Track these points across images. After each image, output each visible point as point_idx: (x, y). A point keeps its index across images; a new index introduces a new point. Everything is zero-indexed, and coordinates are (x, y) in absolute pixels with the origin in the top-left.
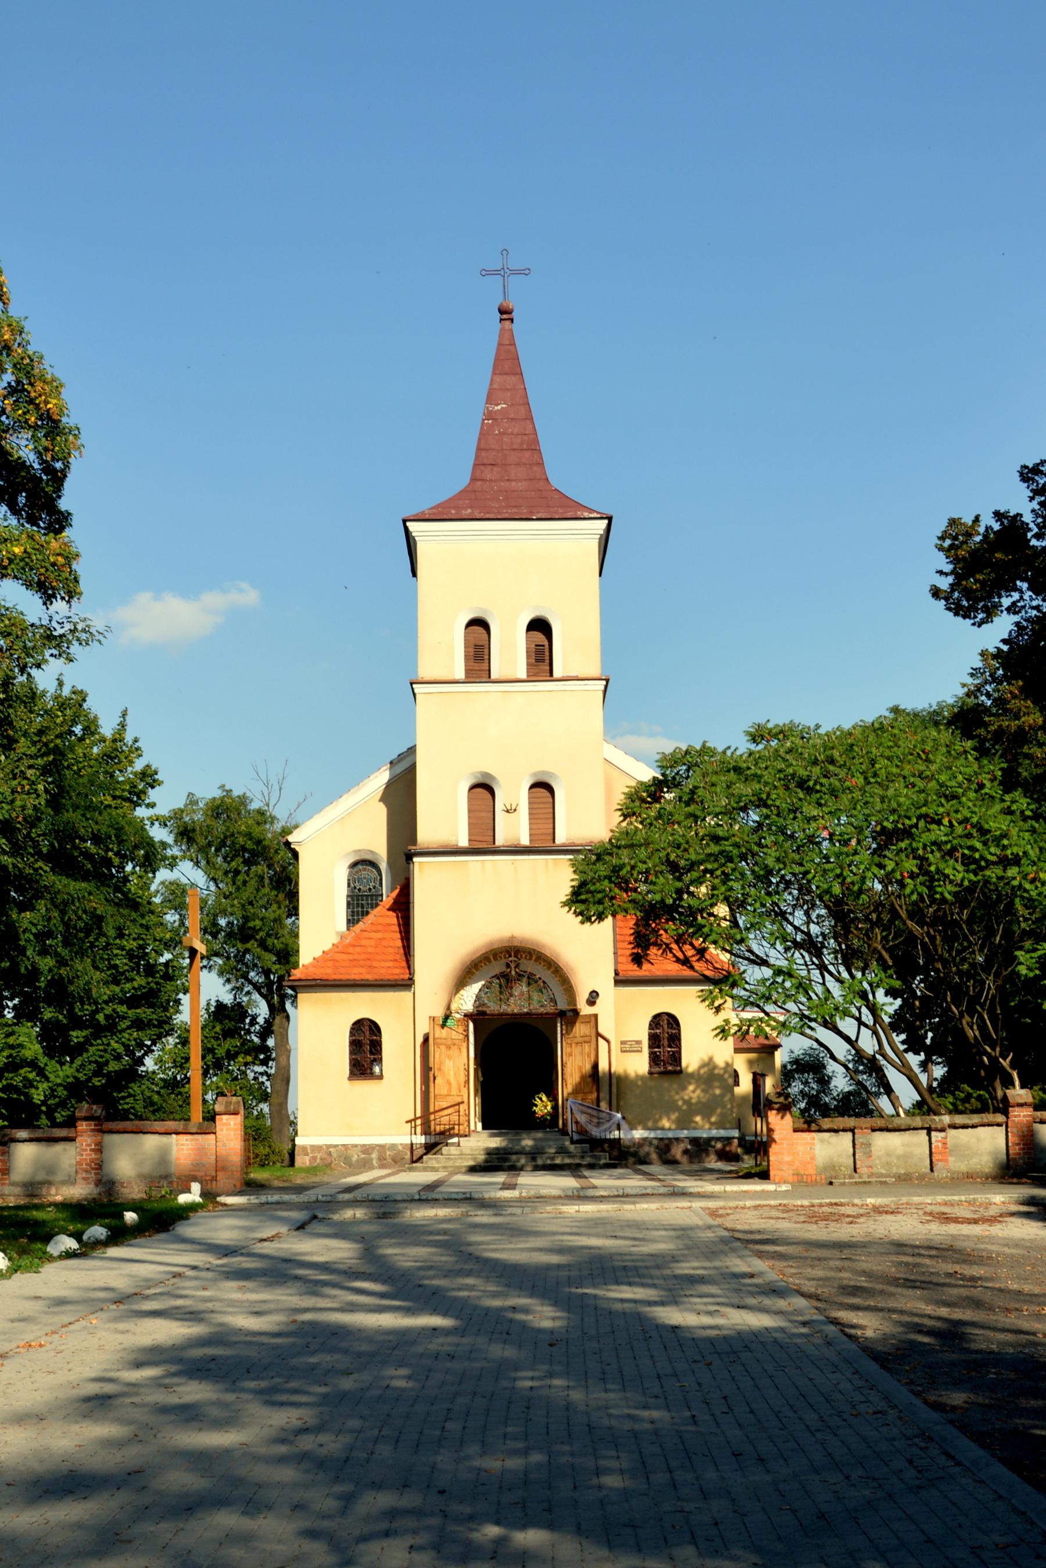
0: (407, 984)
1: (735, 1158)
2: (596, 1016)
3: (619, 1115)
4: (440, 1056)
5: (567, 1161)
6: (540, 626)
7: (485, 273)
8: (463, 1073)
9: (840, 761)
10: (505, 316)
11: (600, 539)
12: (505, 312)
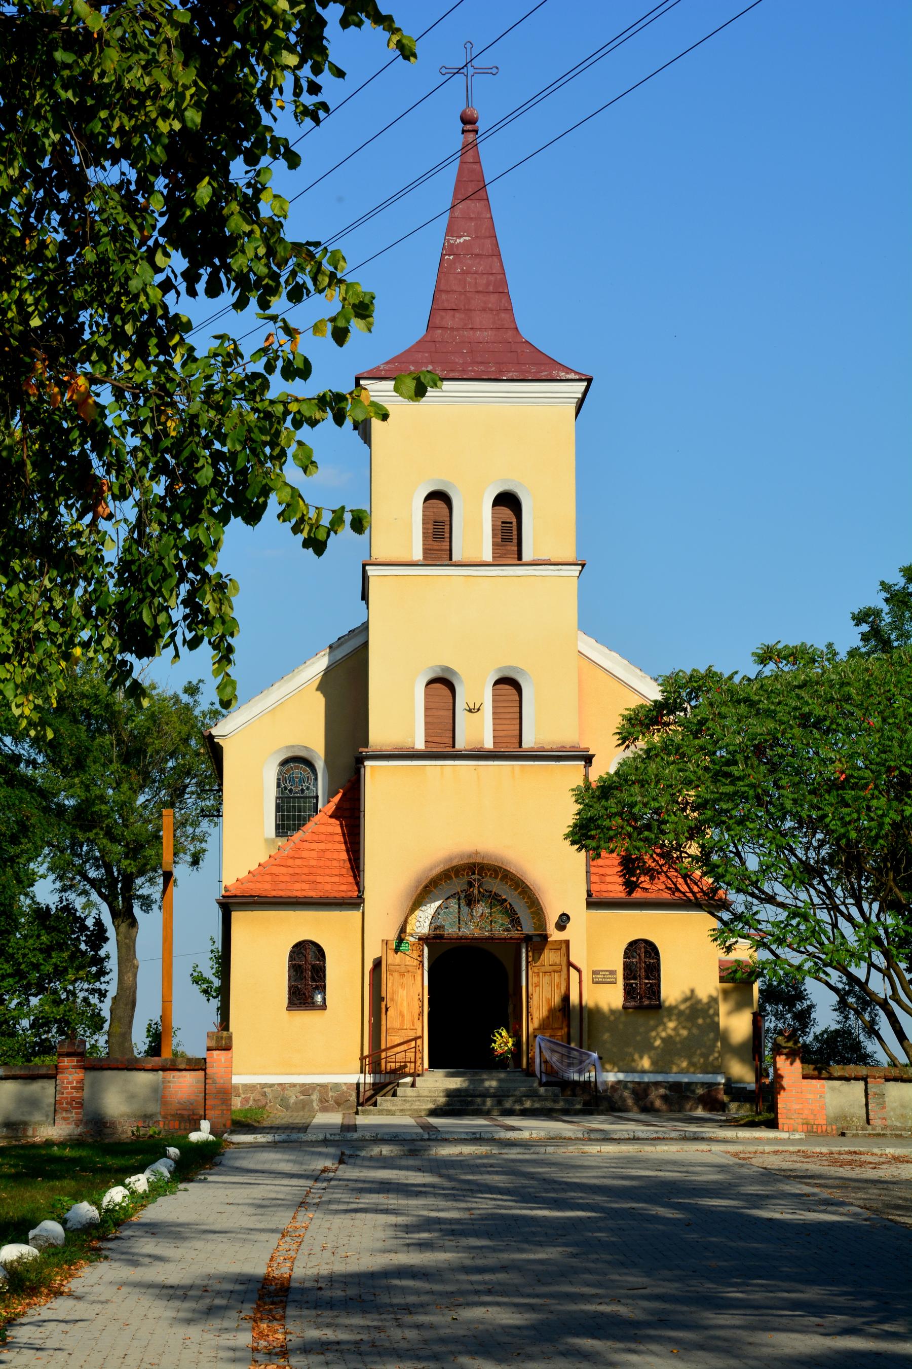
0: (355, 902)
1: (722, 1107)
2: (567, 942)
3: (595, 1055)
4: (393, 984)
5: (537, 1105)
6: (508, 501)
8: (417, 1004)
9: (858, 699)
10: (468, 127)
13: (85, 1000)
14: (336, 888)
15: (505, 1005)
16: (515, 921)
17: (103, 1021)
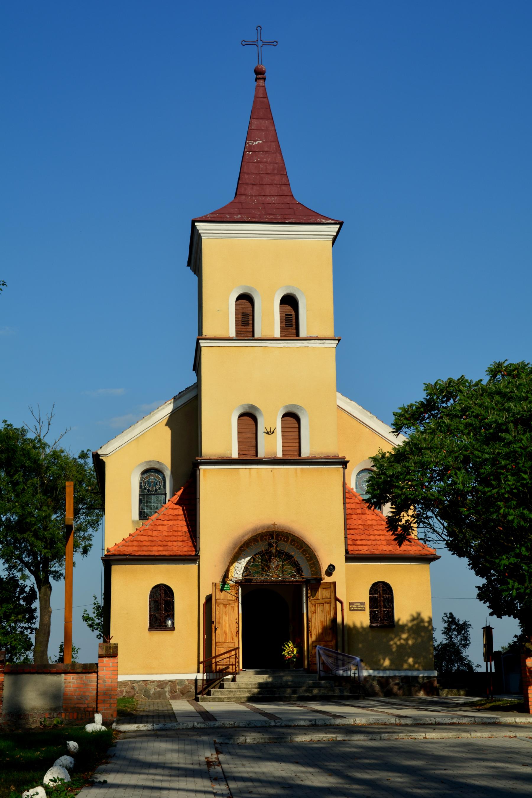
0: (193, 558)
2: (334, 583)
4: (219, 613)
6: (290, 301)
7: (245, 43)
8: (235, 626)
10: (260, 76)
12: (259, 73)
13: (22, 633)
14: (181, 549)
16: (299, 571)
17: (32, 645)
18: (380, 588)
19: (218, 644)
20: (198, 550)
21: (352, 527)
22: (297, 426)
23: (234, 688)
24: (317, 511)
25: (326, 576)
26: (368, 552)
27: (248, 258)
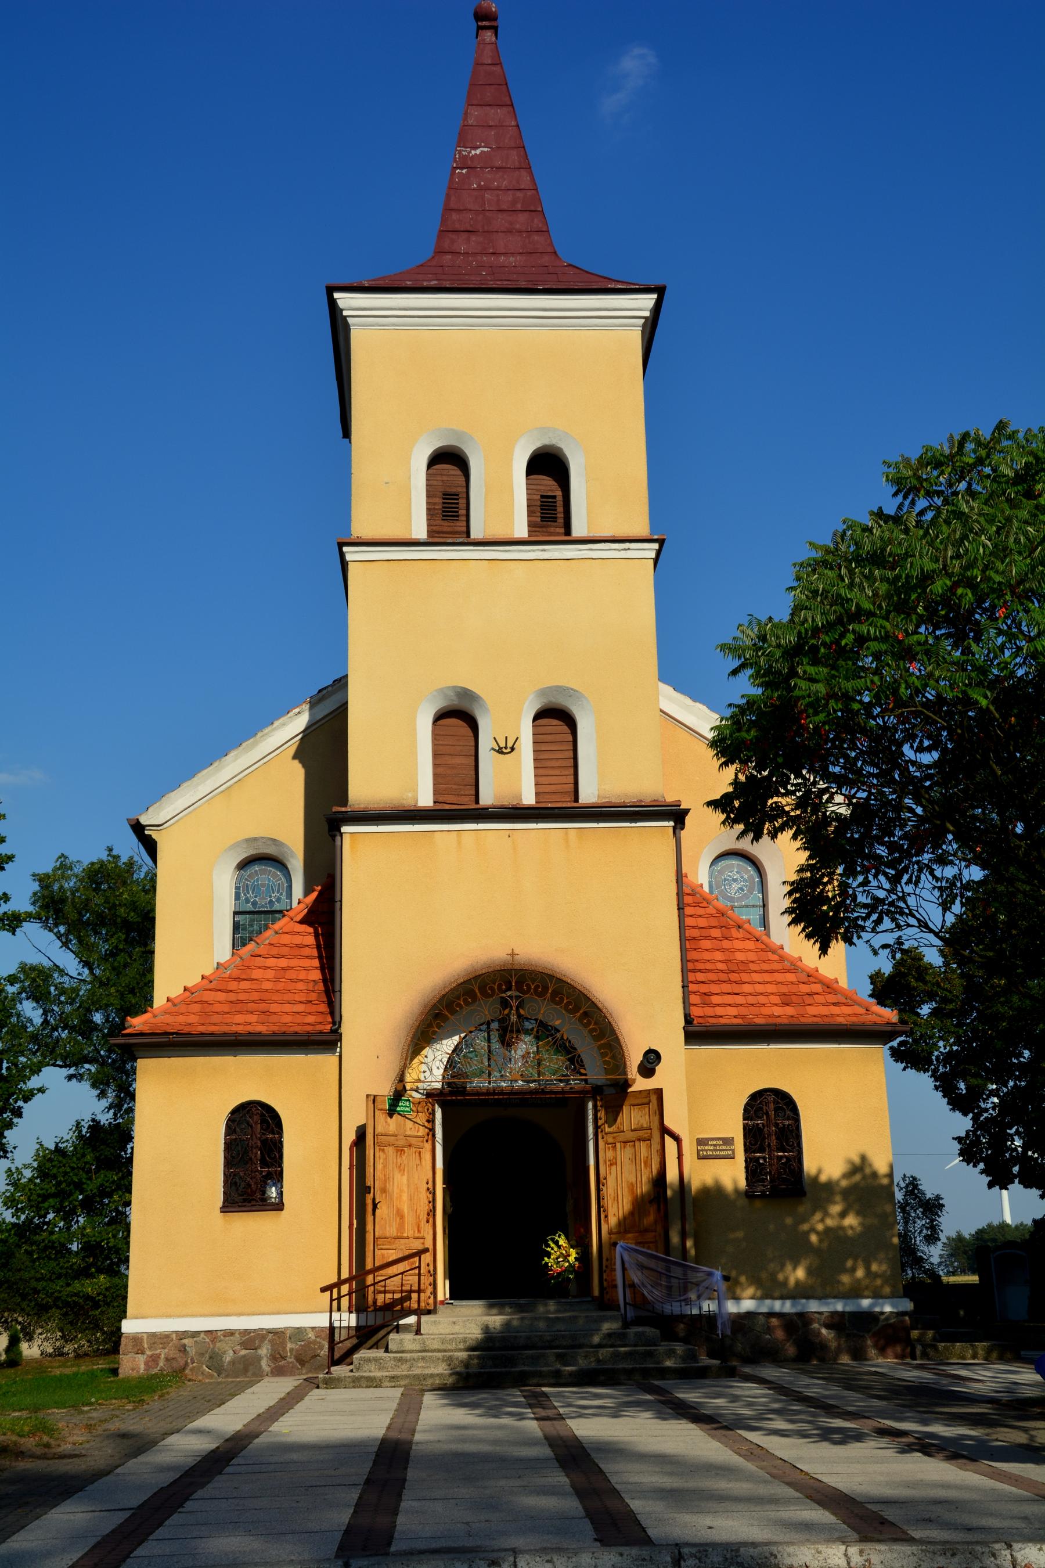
0: (328, 1041)
2: (659, 1093)
4: (385, 1166)
6: (548, 466)
8: (424, 1197)
11: (644, 326)
14: (299, 1019)
15: (566, 1197)
16: (575, 1062)
18: (767, 1104)
19: (380, 1241)
20: (337, 1019)
21: (700, 966)
22: (571, 739)
23: (411, 1352)
24: (608, 920)
25: (639, 1078)
26: (739, 1021)
27: (454, 370)
